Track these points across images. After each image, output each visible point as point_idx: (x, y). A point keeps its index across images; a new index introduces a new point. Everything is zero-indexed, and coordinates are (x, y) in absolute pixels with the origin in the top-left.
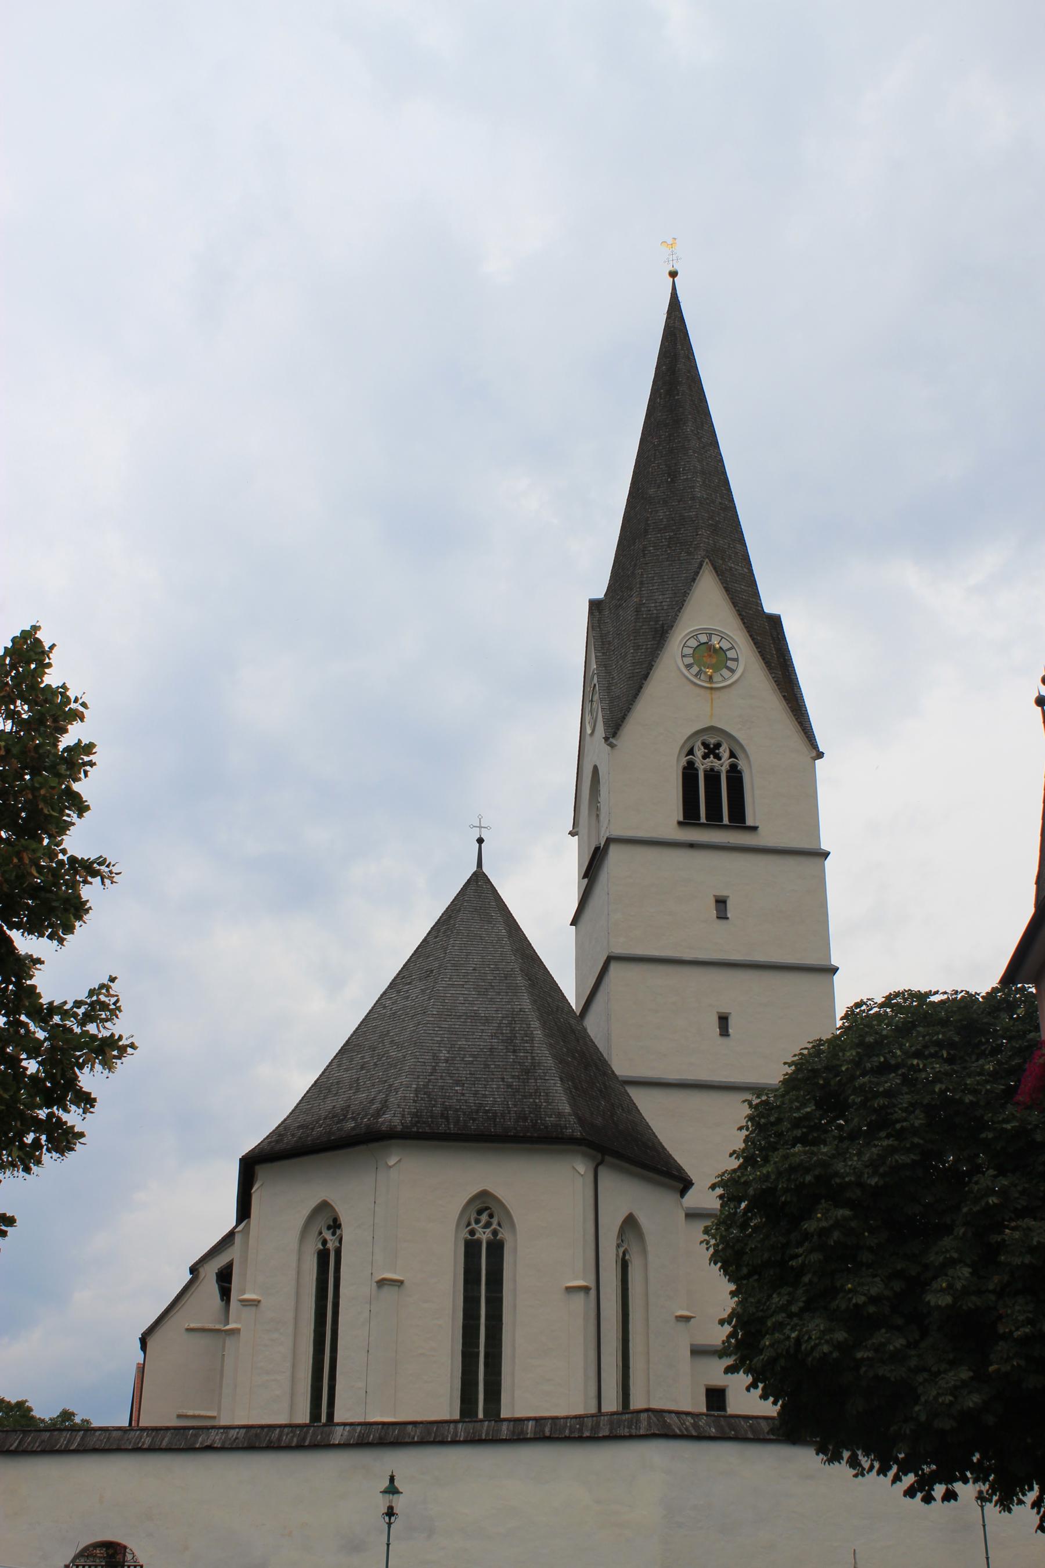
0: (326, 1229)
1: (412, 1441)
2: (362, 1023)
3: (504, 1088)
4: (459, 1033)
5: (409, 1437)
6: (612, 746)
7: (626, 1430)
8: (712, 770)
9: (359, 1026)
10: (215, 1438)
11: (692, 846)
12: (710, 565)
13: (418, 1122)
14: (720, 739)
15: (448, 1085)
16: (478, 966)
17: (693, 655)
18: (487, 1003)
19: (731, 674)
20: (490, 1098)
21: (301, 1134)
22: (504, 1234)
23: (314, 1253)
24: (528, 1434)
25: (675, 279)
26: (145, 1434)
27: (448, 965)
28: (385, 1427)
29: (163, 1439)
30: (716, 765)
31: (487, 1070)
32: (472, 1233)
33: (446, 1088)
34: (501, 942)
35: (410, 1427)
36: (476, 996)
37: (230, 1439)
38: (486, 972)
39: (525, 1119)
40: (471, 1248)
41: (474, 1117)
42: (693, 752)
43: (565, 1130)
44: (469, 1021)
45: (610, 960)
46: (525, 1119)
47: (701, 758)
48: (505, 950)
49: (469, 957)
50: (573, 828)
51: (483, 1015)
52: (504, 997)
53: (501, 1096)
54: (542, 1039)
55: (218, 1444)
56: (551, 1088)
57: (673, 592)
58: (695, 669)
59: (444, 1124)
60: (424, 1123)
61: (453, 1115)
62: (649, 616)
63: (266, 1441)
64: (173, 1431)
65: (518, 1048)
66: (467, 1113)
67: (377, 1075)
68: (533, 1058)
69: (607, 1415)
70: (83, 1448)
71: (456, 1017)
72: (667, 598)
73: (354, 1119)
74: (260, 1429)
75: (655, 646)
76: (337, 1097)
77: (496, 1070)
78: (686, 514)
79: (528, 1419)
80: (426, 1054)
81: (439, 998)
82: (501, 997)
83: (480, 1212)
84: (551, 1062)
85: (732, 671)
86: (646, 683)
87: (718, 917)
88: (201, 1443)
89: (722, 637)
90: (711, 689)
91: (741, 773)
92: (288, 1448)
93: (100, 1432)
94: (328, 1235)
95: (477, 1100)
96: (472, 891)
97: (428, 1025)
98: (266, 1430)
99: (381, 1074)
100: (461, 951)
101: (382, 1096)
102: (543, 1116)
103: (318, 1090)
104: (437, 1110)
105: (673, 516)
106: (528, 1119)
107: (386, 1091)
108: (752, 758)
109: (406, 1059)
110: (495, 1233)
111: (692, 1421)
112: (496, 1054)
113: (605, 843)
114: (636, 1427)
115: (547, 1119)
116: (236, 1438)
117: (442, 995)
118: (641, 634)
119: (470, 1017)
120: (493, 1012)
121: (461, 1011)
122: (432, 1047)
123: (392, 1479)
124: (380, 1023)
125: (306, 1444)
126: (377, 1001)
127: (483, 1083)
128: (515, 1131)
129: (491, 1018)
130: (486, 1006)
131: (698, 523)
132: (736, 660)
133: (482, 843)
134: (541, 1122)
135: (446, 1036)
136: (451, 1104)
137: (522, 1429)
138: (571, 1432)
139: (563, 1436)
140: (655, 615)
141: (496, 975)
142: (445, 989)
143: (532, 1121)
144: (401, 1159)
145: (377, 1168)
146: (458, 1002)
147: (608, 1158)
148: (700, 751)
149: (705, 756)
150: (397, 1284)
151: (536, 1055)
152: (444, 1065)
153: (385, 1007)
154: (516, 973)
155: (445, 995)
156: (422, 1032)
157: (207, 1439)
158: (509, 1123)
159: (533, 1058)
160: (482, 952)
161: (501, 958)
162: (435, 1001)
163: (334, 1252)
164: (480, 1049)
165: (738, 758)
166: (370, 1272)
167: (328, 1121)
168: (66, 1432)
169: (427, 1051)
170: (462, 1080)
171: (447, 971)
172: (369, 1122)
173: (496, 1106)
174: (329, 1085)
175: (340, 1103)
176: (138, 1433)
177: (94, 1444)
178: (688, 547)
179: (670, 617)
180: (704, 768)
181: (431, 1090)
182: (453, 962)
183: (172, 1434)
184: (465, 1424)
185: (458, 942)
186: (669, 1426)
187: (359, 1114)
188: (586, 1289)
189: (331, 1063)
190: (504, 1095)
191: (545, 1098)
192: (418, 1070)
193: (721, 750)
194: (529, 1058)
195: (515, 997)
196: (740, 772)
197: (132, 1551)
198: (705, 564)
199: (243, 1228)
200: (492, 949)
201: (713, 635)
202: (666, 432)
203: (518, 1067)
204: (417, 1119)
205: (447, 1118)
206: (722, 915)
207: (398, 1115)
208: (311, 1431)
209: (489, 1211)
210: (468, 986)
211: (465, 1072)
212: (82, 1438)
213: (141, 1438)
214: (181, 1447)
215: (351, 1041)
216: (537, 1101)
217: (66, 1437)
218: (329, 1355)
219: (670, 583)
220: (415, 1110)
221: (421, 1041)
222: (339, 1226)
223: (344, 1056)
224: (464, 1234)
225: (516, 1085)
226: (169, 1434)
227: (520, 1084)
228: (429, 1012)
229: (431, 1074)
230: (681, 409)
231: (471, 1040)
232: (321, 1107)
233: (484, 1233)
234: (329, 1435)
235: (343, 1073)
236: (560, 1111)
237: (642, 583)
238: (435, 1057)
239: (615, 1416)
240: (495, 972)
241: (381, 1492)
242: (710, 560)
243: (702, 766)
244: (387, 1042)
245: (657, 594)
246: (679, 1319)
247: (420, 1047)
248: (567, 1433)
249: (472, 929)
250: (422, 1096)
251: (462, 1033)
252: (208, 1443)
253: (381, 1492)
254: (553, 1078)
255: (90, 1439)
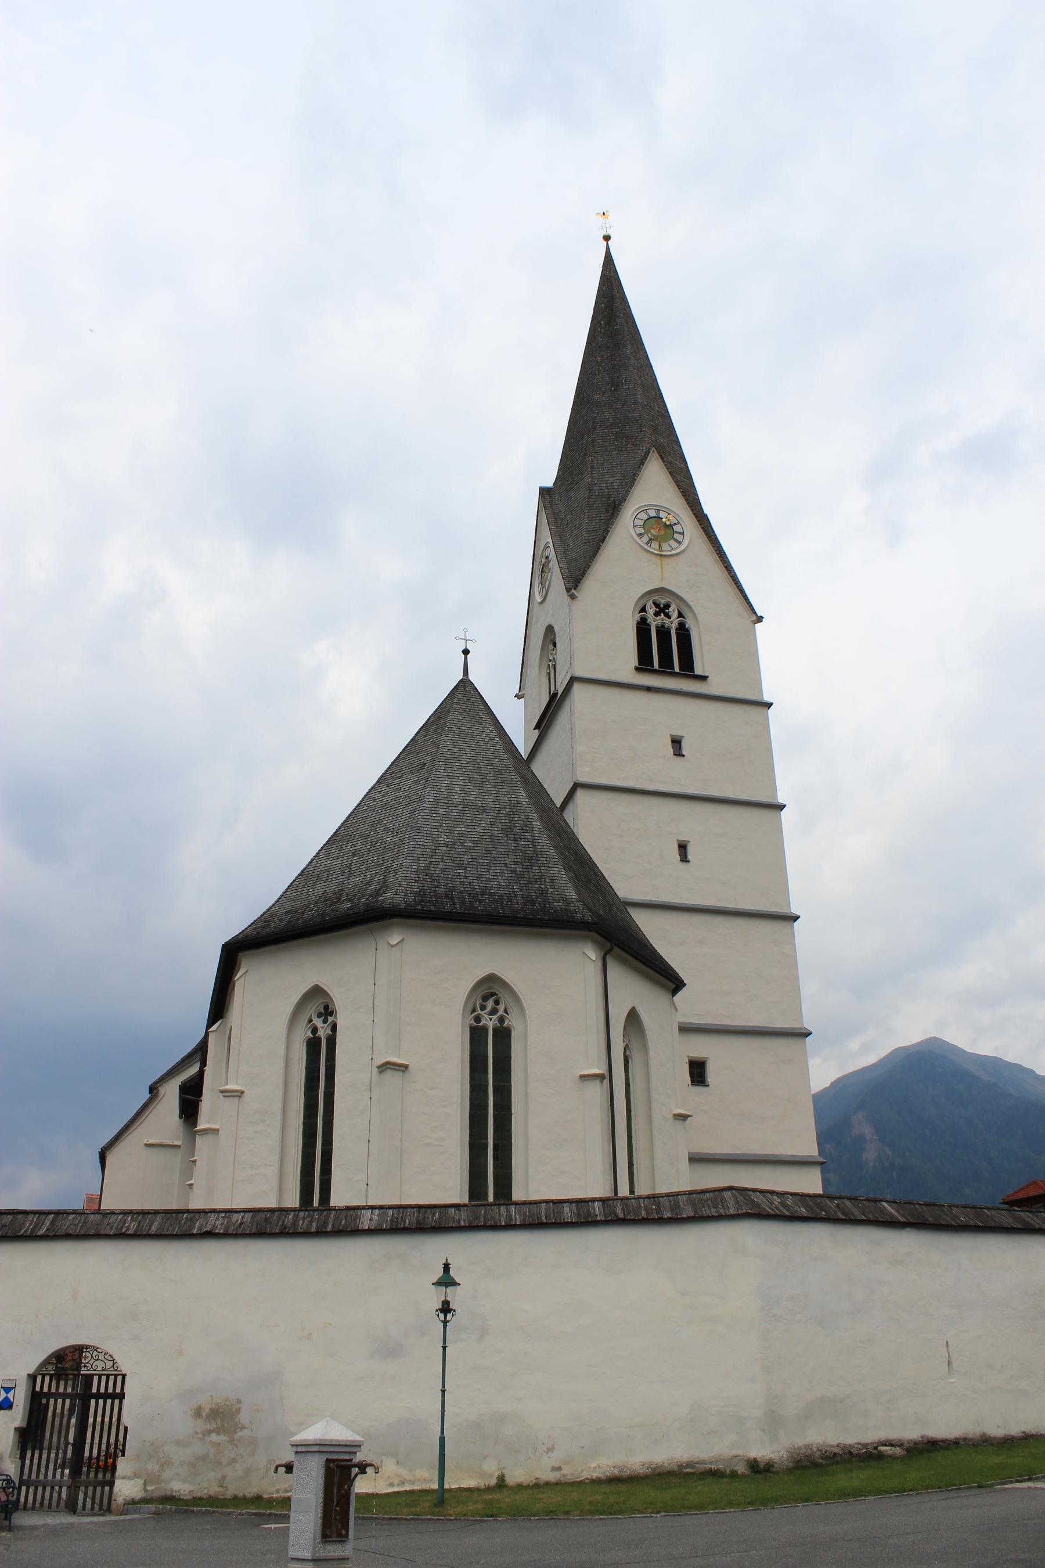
0: (316, 1015)
1: (458, 1225)
2: (350, 815)
3: (508, 874)
4: (458, 820)
5: (454, 1222)
6: (573, 597)
7: (713, 1210)
8: (663, 626)
9: (347, 818)
10: (215, 1224)
11: (649, 689)
12: (656, 453)
13: (422, 901)
14: (669, 600)
15: (450, 867)
16: (472, 761)
17: (644, 526)
18: (483, 794)
19: (678, 545)
20: (494, 882)
21: (290, 919)
22: (513, 1021)
23: (303, 1042)
24: (597, 1216)
25: (609, 242)
26: (130, 1218)
27: (442, 758)
28: (422, 1211)
29: (152, 1224)
30: (667, 622)
31: (489, 855)
32: (478, 1019)
33: (448, 870)
34: (493, 741)
35: (452, 1210)
36: (472, 787)
37: (234, 1224)
38: (480, 766)
39: (533, 903)
40: (477, 1035)
41: (480, 898)
42: (645, 610)
43: (574, 915)
44: (467, 809)
45: (576, 786)
46: (533, 903)
47: (652, 614)
48: (497, 748)
49: (462, 752)
50: (519, 691)
51: (481, 805)
52: (500, 790)
53: (505, 881)
54: (542, 830)
55: (220, 1230)
56: (556, 875)
57: (622, 475)
58: (646, 539)
59: (450, 904)
60: (428, 902)
61: (458, 896)
62: (601, 494)
63: (279, 1226)
64: (164, 1215)
65: (518, 837)
66: (472, 895)
67: (372, 859)
68: (534, 847)
69: (684, 1194)
70: (54, 1233)
71: (454, 805)
72: (617, 480)
73: (349, 900)
74: (269, 1213)
75: (608, 517)
76: (328, 883)
77: (498, 856)
78: (630, 415)
79: (593, 1200)
80: (425, 838)
81: (435, 787)
82: (497, 790)
83: (485, 998)
84: (553, 851)
85: (679, 543)
86: (603, 545)
87: (674, 754)
88: (198, 1229)
89: (609, 1077)
90: (661, 555)
91: (689, 632)
92: (307, 1234)
93: (74, 1216)
94: (318, 1022)
95: (481, 883)
96: (460, 695)
97: (426, 811)
98: (277, 1214)
99: (376, 858)
100: (454, 746)
101: (379, 878)
102: (550, 901)
103: (306, 878)
104: (441, 890)
105: (619, 416)
106: (535, 903)
107: (384, 873)
108: (700, 618)
109: (404, 842)
110: (501, 1020)
111: (779, 1201)
112: (497, 841)
113: (562, 694)
114: (723, 1206)
115: (555, 904)
116: (241, 1224)
117: (438, 784)
118: (594, 508)
119: (468, 806)
120: (490, 803)
121: (458, 800)
122: (430, 831)
123: (447, 1267)
124: (371, 814)
125: (329, 1229)
126: (365, 796)
127: (486, 867)
128: (524, 913)
129: (489, 808)
130: (483, 797)
131: (641, 422)
132: (682, 533)
133: (468, 654)
134: (549, 907)
135: (444, 822)
136: (454, 886)
137: (588, 1211)
138: (648, 1213)
139: (640, 1218)
140: (606, 493)
141: (490, 770)
142: (440, 779)
143: (539, 904)
144: (403, 939)
145: (376, 949)
146: (454, 791)
147: (616, 949)
148: (652, 610)
149: (657, 614)
150: (401, 1068)
151: (537, 844)
152: (445, 848)
153: (374, 800)
154: (510, 769)
155: (440, 785)
156: (420, 817)
157: (206, 1224)
158: (517, 906)
159: (534, 847)
160: (475, 748)
161: (493, 755)
162: (430, 789)
163: (325, 1040)
164: (480, 835)
165: (685, 615)
166: (371, 1057)
167: (320, 905)
168: (33, 1215)
169: (426, 835)
170: (464, 864)
171: (441, 763)
172: (367, 901)
173: (501, 889)
174: (318, 873)
175: (332, 887)
176: (121, 1216)
177: (67, 1229)
178: (633, 440)
179: (621, 495)
180: (656, 624)
181: (432, 872)
182: (446, 756)
183: (163, 1218)
184: (517, 1206)
185: (451, 738)
186: (758, 1205)
187: (355, 896)
188: (600, 1077)
189: (318, 853)
190: (508, 880)
191: (551, 884)
192: (417, 852)
193: (670, 609)
194: (531, 846)
195: (511, 791)
196: (688, 630)
197: (111, 1357)
198: (652, 451)
199: (217, 1028)
200: (485, 747)
201: (660, 511)
202: (607, 353)
203: (521, 854)
204: (420, 898)
205: (452, 899)
206: (678, 752)
207: (400, 894)
208: (332, 1216)
209: (495, 997)
210: (463, 778)
211: (466, 857)
212: (52, 1223)
213: (125, 1223)
214: (175, 1233)
215: (339, 832)
216: (543, 887)
217: (32, 1221)
218: (320, 1148)
219: (619, 468)
220: (418, 890)
221: (419, 825)
222: (331, 1014)
223: (333, 846)
224: (470, 1020)
225: (520, 871)
226: (159, 1218)
227: (524, 870)
228: (426, 800)
229: (432, 857)
230: (620, 336)
231: (470, 827)
232: (310, 893)
233: (491, 1020)
234: (355, 1220)
235: (332, 862)
236: (567, 897)
237: (592, 467)
238: (434, 841)
239: (694, 1195)
240: (489, 767)
241: (433, 1284)
242: (656, 449)
243: (654, 622)
244: (379, 830)
245: (607, 476)
246: (676, 1117)
247: (419, 831)
248: (644, 1214)
249: (463, 728)
250: (424, 877)
251: (461, 820)
252: (208, 1228)
253: (433, 1284)
254: (557, 866)
255: (62, 1224)
